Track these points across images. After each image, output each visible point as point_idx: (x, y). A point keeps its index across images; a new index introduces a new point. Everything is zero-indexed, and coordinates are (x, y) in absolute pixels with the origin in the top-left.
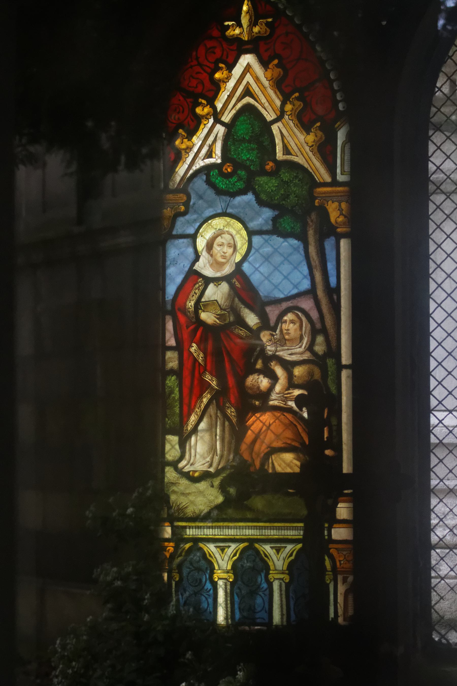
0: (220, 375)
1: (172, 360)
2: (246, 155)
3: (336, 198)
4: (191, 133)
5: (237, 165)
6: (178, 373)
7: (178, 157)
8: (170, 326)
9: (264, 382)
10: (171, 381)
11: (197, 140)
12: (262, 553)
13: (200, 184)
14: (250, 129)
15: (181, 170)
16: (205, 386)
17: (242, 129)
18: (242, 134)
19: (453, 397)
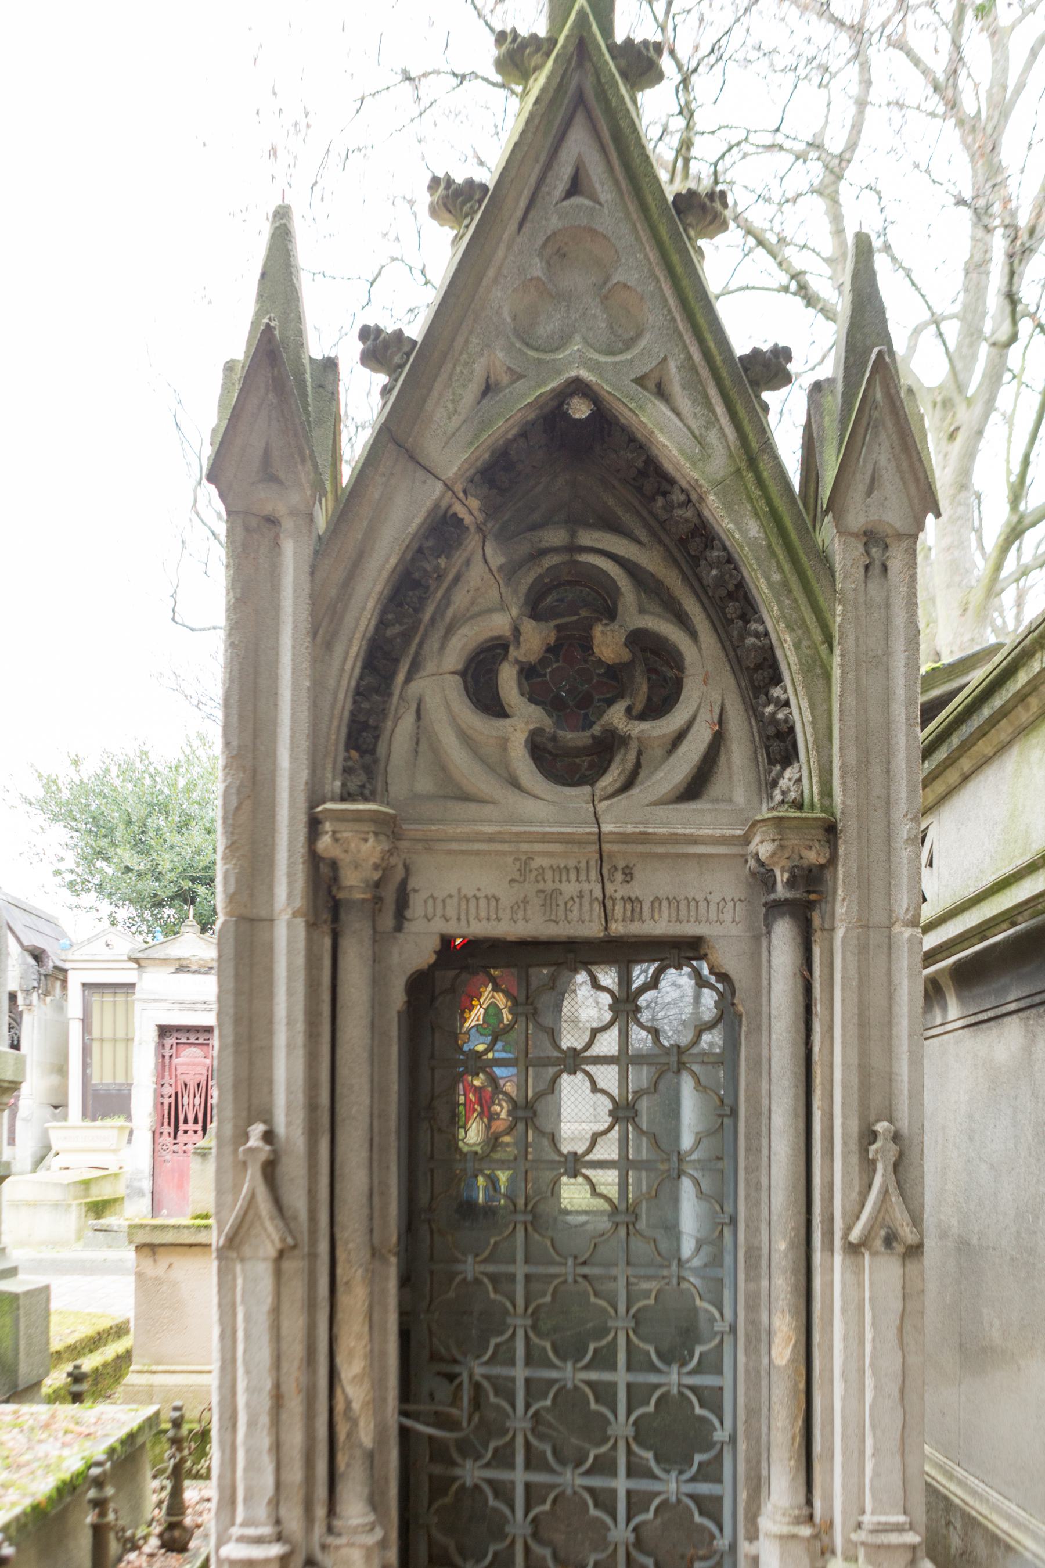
0: (481, 1106)
1: (462, 1099)
2: (492, 1021)
3: (558, 848)
4: (471, 1011)
5: (489, 1025)
6: (465, 1105)
7: (465, 1020)
8: (461, 1086)
9: (498, 1109)
10: (461, 1108)
11: (473, 1014)
12: (642, 534)
13: (474, 1030)
14: (493, 1011)
15: (467, 1025)
16: (475, 1110)
17: (491, 1011)
18: (775, 1522)
19: (899, 1466)
